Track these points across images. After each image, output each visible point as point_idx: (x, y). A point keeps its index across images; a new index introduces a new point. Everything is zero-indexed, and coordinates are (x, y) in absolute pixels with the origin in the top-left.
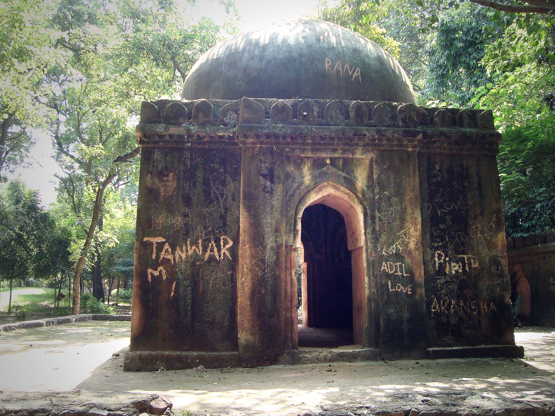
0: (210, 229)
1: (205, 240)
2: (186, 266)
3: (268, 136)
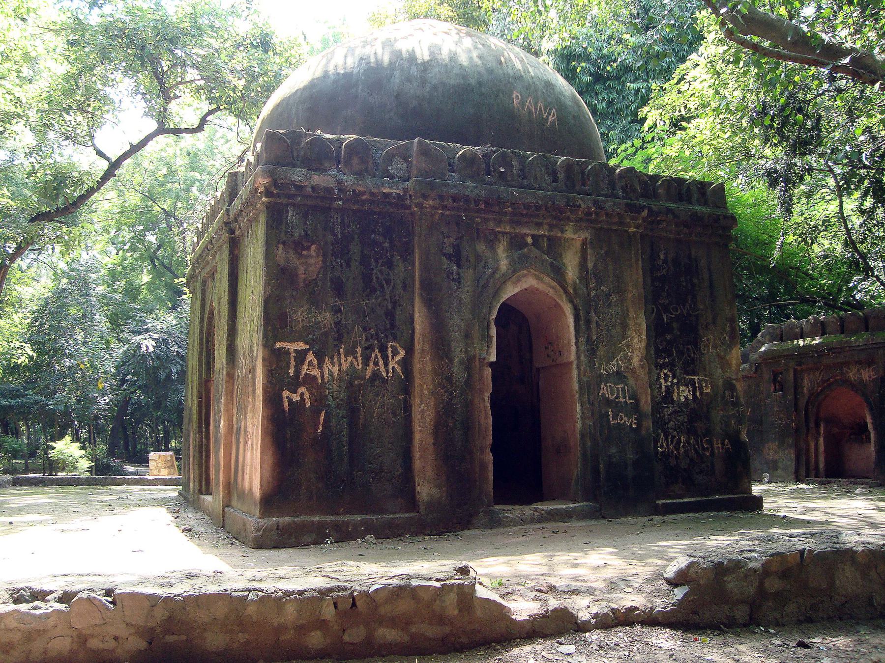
1: (366, 348)
2: (339, 387)
3: (455, 199)
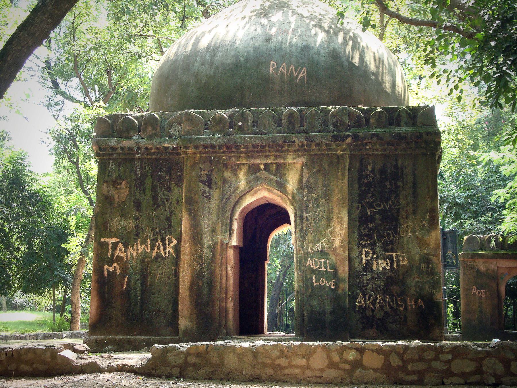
0: (157, 230)
1: (153, 240)
2: (136, 262)
3: (205, 147)
